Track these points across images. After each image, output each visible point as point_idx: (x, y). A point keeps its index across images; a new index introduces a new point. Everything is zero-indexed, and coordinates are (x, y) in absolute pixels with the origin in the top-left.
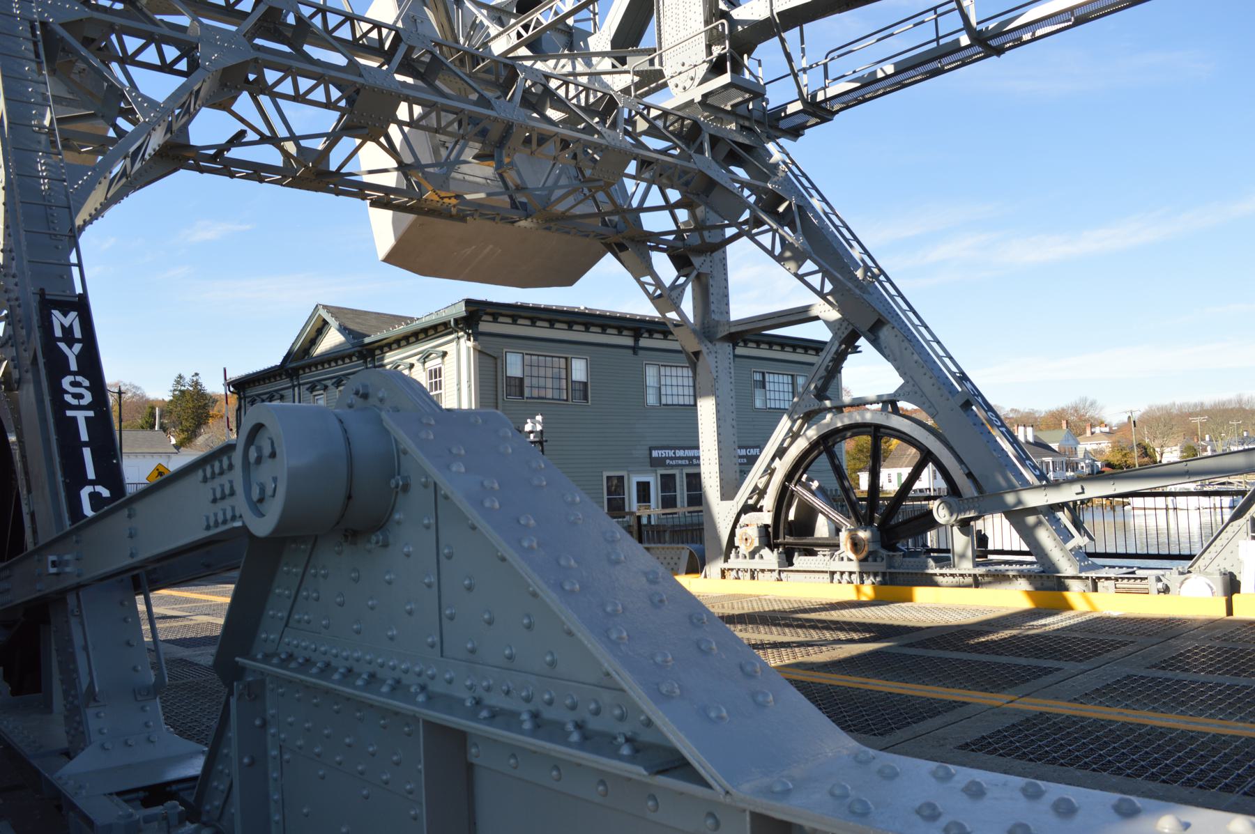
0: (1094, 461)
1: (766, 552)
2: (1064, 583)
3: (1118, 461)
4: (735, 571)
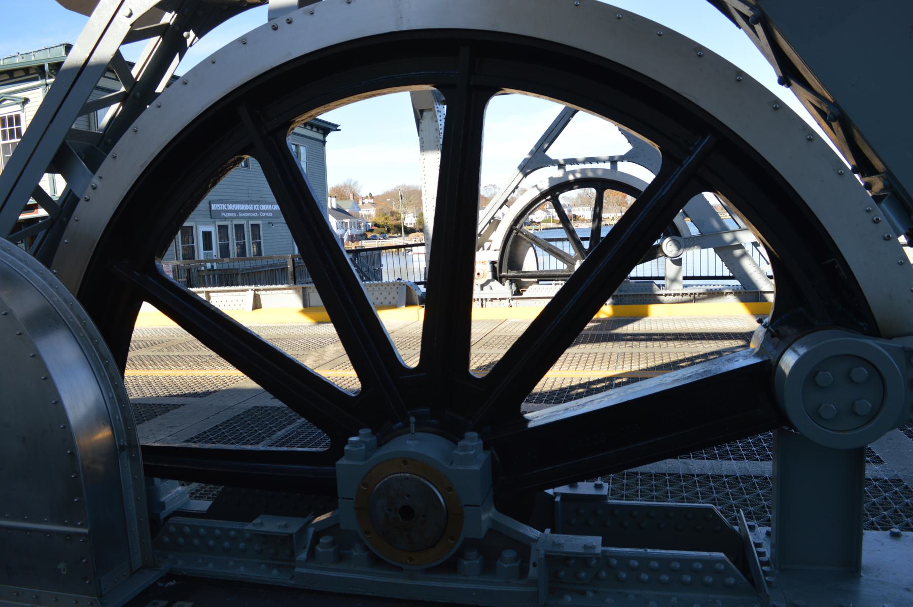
0: (367, 222)
1: (496, 284)
2: (763, 296)
3: (382, 222)
4: (507, 300)
